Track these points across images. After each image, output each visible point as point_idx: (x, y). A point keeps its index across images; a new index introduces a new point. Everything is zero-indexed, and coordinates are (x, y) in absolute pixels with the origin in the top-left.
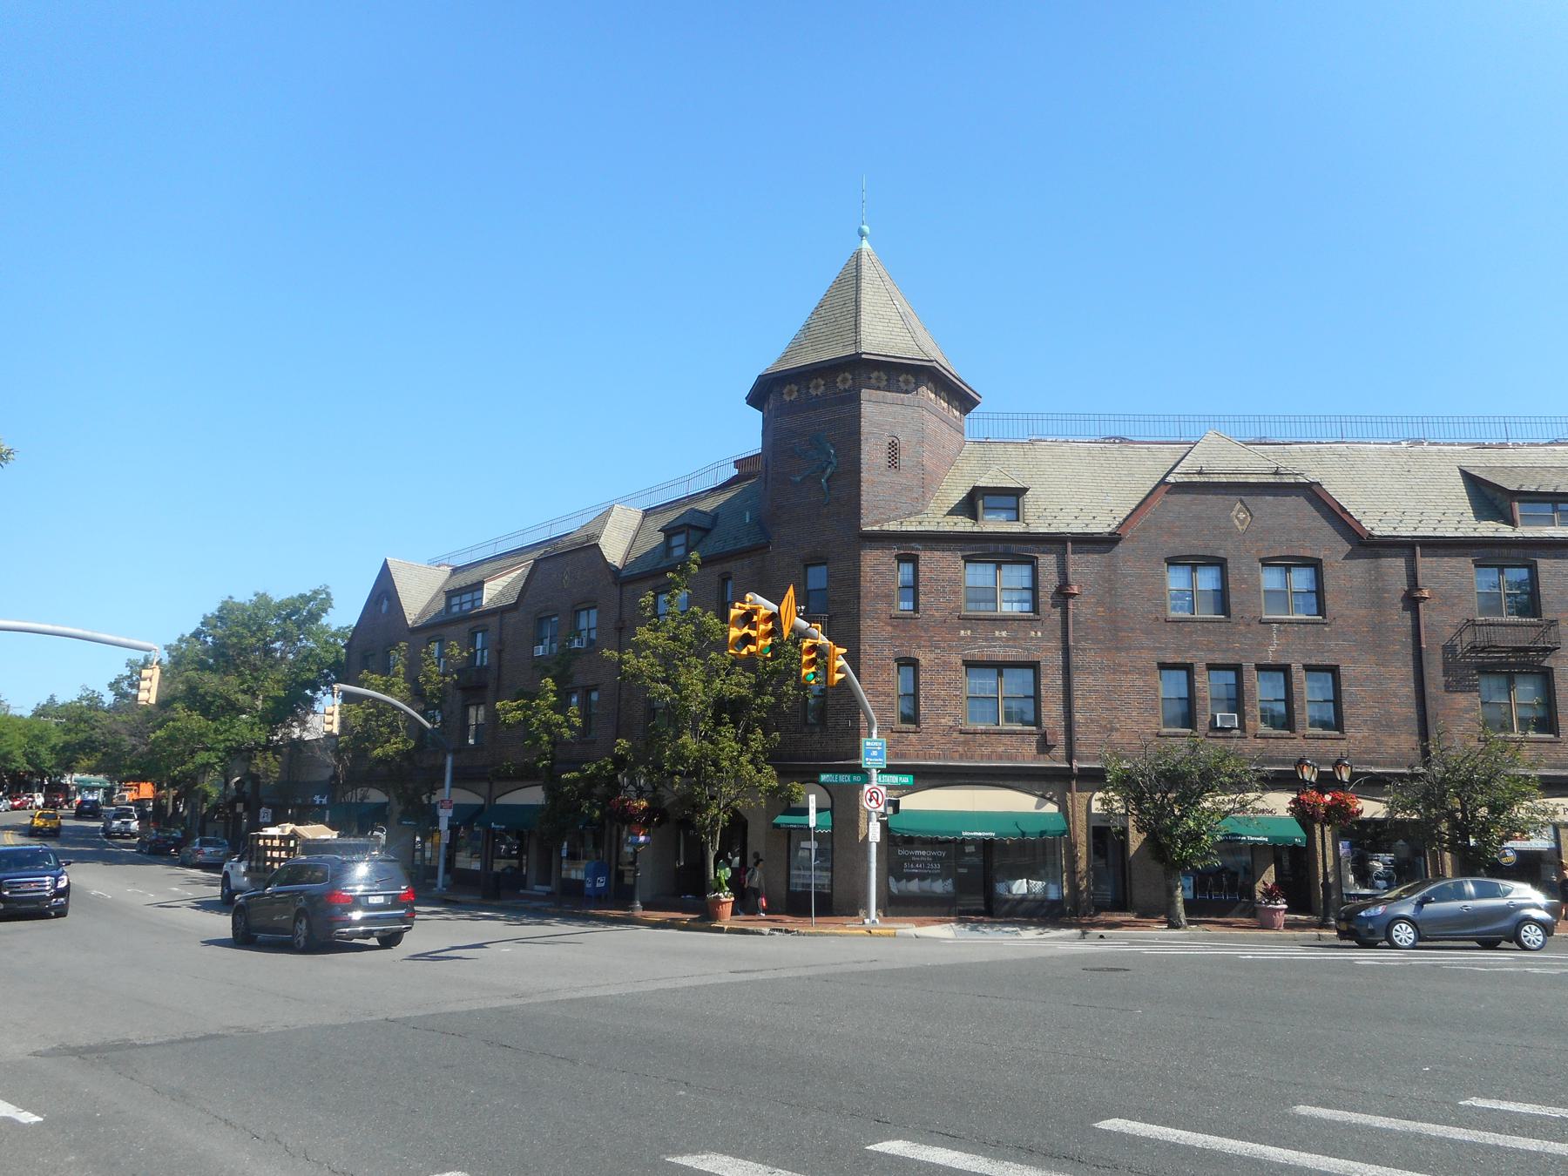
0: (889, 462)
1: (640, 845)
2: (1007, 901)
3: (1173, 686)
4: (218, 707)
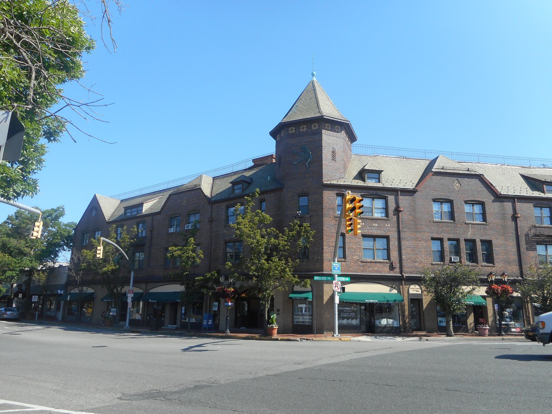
0: (332, 158)
1: (229, 306)
2: (380, 327)
3: (436, 246)
4: (15, 253)
